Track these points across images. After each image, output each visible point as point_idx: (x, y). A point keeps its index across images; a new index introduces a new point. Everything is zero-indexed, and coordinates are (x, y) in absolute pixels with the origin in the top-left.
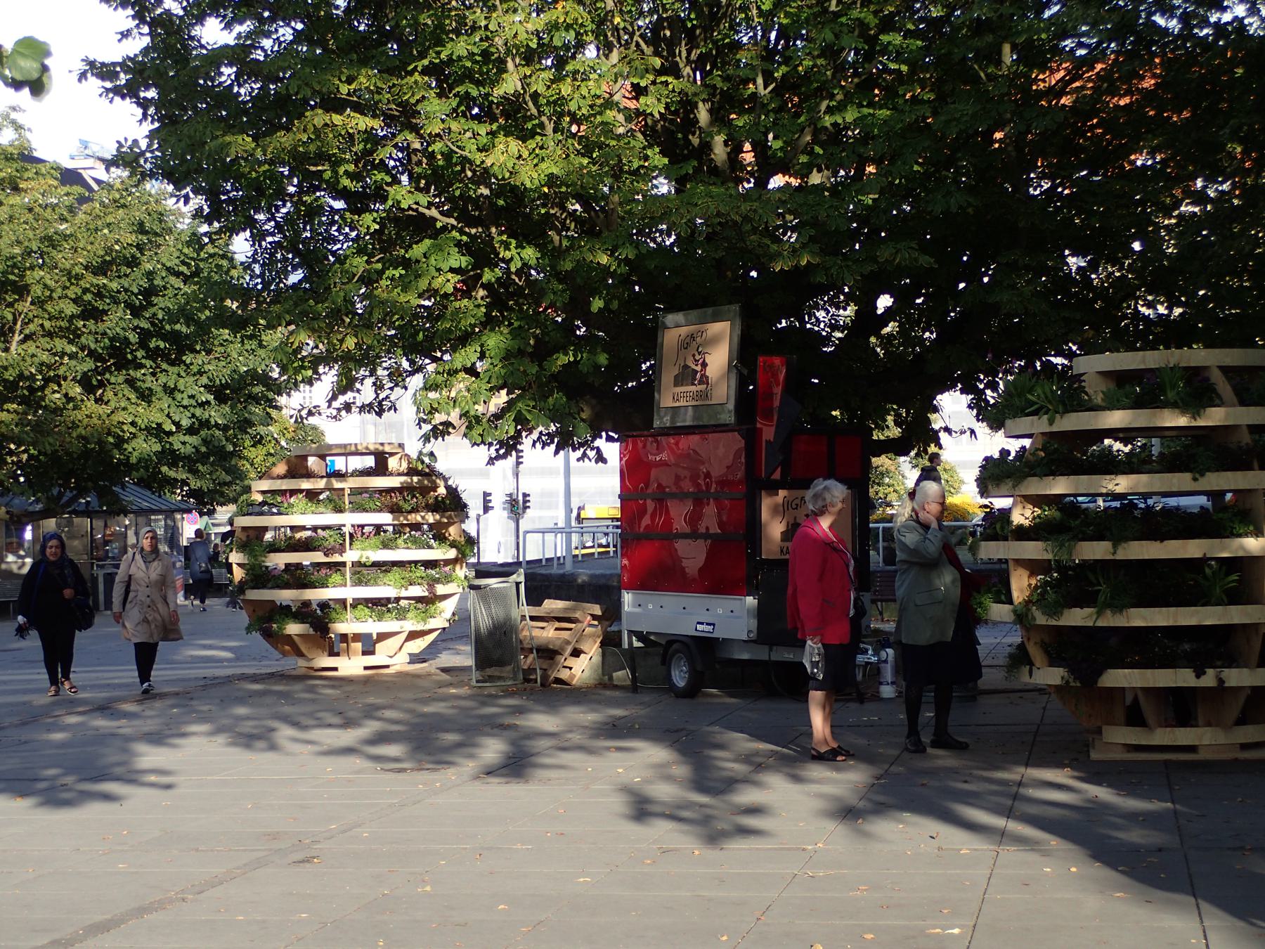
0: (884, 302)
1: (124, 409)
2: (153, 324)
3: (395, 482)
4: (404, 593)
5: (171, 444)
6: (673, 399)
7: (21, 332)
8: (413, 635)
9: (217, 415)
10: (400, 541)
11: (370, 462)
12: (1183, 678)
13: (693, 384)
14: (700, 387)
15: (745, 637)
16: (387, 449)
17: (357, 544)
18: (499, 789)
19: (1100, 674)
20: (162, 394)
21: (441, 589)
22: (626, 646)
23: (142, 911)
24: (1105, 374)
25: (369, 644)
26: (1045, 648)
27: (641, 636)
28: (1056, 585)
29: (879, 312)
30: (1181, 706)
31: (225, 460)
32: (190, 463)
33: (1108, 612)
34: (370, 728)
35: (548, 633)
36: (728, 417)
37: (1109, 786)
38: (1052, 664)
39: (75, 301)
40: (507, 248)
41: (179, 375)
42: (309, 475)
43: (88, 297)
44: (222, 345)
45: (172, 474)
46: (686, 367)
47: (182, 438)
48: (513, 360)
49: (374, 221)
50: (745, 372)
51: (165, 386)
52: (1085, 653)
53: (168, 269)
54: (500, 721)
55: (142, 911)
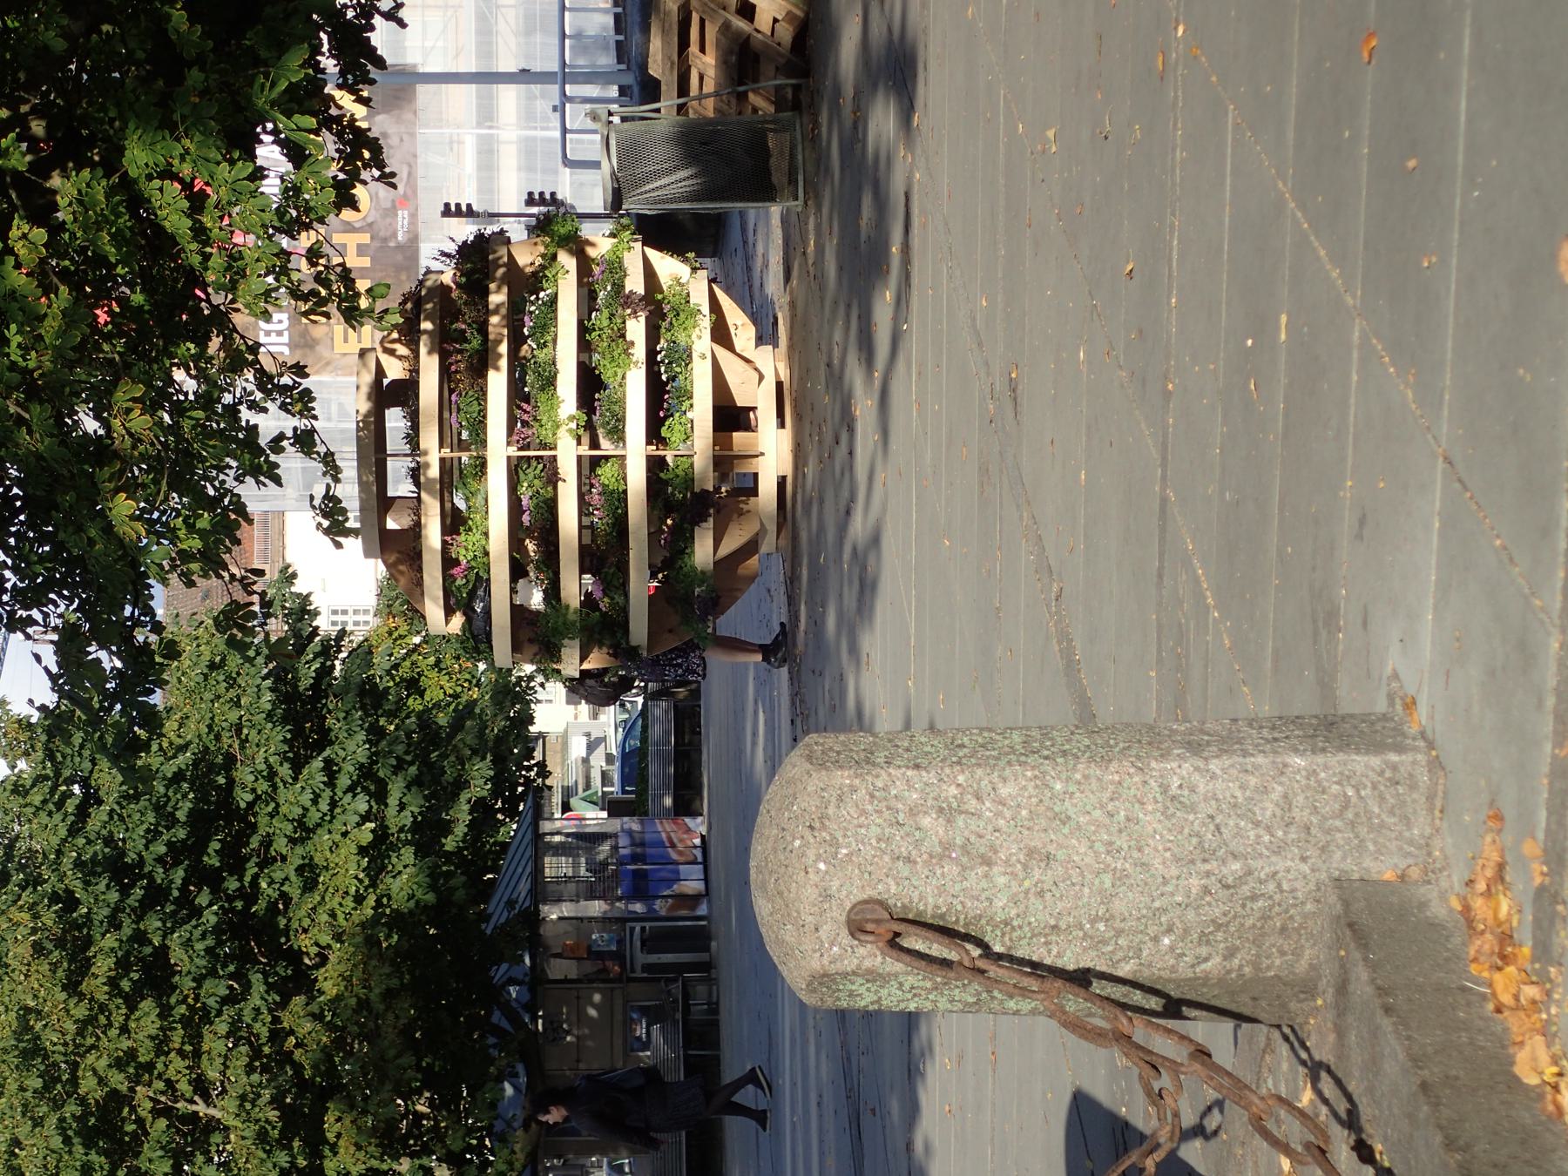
1: (333, 915)
2: (176, 863)
3: (430, 369)
4: (639, 352)
5: (401, 830)
7: (192, 1102)
8: (721, 334)
9: (353, 749)
10: (542, 355)
16: (368, 378)
18: (936, 84)
20: (309, 846)
21: (635, 283)
23: (1071, 667)
25: (731, 418)
31: (437, 734)
32: (439, 790)
34: (855, 375)
35: (706, 64)
39: (132, 1008)
41: (271, 816)
43: (126, 985)
44: (218, 737)
45: (460, 830)
47: (392, 811)
48: (177, 117)
53: (73, 831)
54: (848, 123)
55: (1071, 667)
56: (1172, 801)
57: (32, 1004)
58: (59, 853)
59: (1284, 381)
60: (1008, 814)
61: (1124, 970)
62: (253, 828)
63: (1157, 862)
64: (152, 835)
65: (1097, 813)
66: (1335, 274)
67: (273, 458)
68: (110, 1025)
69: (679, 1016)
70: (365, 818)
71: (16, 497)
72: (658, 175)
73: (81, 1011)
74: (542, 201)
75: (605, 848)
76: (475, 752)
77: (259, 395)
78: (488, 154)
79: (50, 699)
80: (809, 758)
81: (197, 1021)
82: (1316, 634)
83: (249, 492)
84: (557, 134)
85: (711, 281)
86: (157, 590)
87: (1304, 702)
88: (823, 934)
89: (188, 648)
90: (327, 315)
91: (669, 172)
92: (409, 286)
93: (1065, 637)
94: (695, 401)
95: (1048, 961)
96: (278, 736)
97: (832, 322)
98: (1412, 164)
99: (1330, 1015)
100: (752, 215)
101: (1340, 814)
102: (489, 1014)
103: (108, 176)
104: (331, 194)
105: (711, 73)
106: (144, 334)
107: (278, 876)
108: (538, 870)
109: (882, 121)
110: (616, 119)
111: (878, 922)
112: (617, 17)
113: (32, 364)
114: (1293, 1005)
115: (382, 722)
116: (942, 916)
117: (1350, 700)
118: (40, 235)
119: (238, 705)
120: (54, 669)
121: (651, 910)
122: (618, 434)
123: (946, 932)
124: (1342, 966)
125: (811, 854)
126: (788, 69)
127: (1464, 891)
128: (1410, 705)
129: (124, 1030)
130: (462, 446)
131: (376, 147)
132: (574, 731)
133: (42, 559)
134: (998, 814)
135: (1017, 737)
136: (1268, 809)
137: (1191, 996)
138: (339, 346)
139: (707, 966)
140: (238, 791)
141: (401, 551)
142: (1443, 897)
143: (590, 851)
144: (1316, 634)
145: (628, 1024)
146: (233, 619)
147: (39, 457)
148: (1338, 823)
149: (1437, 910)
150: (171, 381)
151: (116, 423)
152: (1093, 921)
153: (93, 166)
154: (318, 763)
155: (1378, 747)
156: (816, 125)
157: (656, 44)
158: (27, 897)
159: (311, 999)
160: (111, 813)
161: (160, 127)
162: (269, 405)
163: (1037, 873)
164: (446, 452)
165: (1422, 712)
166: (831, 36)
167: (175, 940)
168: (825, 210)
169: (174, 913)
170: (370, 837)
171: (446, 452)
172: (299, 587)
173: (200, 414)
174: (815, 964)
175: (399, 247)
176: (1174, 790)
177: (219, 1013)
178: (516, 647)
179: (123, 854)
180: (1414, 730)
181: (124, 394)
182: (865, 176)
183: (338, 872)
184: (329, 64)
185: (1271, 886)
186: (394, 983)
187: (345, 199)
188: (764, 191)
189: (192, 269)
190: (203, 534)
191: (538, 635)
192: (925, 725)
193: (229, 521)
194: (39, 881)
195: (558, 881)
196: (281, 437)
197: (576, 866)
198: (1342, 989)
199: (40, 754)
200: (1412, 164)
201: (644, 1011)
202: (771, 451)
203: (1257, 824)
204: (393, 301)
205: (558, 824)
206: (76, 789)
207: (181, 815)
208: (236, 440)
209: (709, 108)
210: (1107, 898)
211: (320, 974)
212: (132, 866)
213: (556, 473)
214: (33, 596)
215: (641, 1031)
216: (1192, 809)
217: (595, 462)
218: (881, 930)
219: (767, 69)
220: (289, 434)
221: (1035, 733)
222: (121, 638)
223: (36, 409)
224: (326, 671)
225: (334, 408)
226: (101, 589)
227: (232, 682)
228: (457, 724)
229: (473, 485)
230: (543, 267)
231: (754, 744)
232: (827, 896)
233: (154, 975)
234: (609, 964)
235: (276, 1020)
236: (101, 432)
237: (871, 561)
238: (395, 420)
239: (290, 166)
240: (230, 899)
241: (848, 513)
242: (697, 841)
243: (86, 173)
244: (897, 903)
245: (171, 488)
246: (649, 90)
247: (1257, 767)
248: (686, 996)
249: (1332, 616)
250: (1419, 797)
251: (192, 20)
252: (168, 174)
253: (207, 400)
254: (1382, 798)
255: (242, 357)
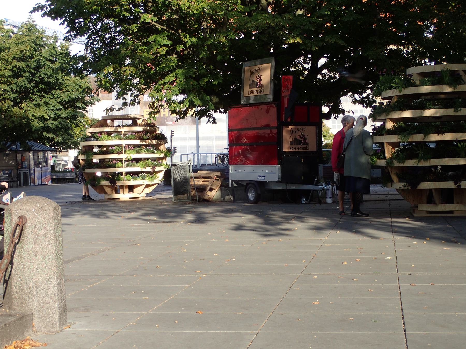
0: (322, 61)
1: (30, 110)
2: (40, 79)
4: (144, 170)
5: (47, 124)
6: (249, 93)
8: (148, 186)
9: (64, 114)
10: (143, 151)
11: (130, 122)
12: (450, 185)
13: (256, 87)
14: (259, 89)
15: (277, 180)
16: (138, 117)
17: (127, 152)
18: (197, 227)
19: (419, 184)
20: (44, 105)
21: (157, 169)
22: (230, 186)
23: (79, 258)
24: (420, 74)
25: (131, 188)
26: (398, 175)
27: (236, 182)
28: (402, 151)
29: (319, 66)
30: (447, 196)
32: (56, 131)
33: (422, 160)
35: (200, 182)
36: (270, 98)
37: (425, 222)
38: (400, 181)
39: (10, 70)
40: (186, 37)
42: (107, 126)
43: (15, 69)
44: (66, 87)
45: (48, 135)
46: (253, 81)
49: (136, 27)
50: (276, 82)
51: (45, 102)
52: (412, 177)
53: (46, 59)
54: (189, 210)
55: (79, 258)
56: (48, 280)
57: (11, 50)
58: (41, 56)
59: (135, 298)
60: (45, 247)
61: (13, 272)
62: (47, 94)
63: (35, 277)
64: (45, 74)
65: (45, 265)
66: (156, 308)
67: (121, 98)
68: (6, 66)
69: (10, 180)
70: (50, 116)
71: (112, 48)
72: (179, 173)
73: (10, 60)
74: (175, 150)
75: (45, 165)
76: (64, 138)
77: (134, 95)
78: (184, 139)
79: (72, 54)
80: (56, 207)
81: (9, 84)
82: (84, 307)
83: (114, 94)
84: (188, 153)
85: (158, 184)
86: (94, 75)
87: (69, 305)
88: (20, 211)
89: (83, 81)
90: (150, 108)
91: (179, 175)
92: (156, 125)
93: (85, 256)
94: (135, 181)
95: (15, 256)
96: (66, 99)
97: (150, 208)
98: (177, 322)
99: (5, 313)
100: (171, 191)
101: (46, 314)
102: (10, 142)
103: (176, 66)
104: (173, 109)
105: (199, 183)
106: (145, 72)
107: (37, 99)
108: (40, 151)
109: (190, 217)
110: (189, 164)
111: (22, 222)
112: (210, 164)
113: (138, 51)
114: (7, 306)
115: (70, 120)
116: (24, 235)
117: (70, 315)
118: (164, 53)
119: (72, 91)
120: (78, 55)
121: (32, 174)
122: (127, 166)
123: (20, 235)
124: (15, 315)
125: (36, 208)
126: (200, 198)
127: (31, 339)
128: (69, 327)
129: (6, 69)
130: (125, 135)
131: (182, 118)
132: (68, 158)
133: (100, 53)
134: (45, 245)
135: (61, 248)
136: (47, 299)
137: (8, 285)
138: (145, 111)
139: (20, 185)
140: (55, 91)
141: (103, 123)
142: (29, 335)
143: (44, 161)
144: (84, 307)
145: (7, 170)
146: (89, 90)
147: (120, 52)
148: (44, 313)
149: (27, 334)
150: (136, 78)
151: (127, 68)
152: (23, 265)
153: (178, 63)
154: (61, 107)
155: (60, 321)
156: (189, 204)
157: (204, 172)
158: (32, 49)
159: (12, 106)
160: (50, 66)
161: (186, 76)
162: (132, 97)
163: (33, 253)
164: (123, 132)
165: (67, 329)
166: (206, 206)
167: (24, 78)
168: (172, 206)
169: (29, 79)
170: (46, 118)
171: (123, 132)
172: (96, 103)
173: (129, 84)
174: (13, 209)
175: (165, 122)
176: (50, 280)
177: (9, 88)
178: (84, 146)
179: (41, 68)
180: (64, 328)
181: (133, 69)
182: (179, 214)
183: (38, 111)
184: (199, 108)
185: (31, 300)
186: (16, 123)
187: (173, 112)
188: (176, 194)
189: (158, 82)
190: (105, 85)
191: (88, 151)
192: (64, 229)
193: (109, 90)
194: (35, 51)
195: (37, 156)
196: (126, 100)
197: (41, 159)
198: (10, 315)
199: (62, 52)
200: (177, 322)
201: (11, 173)
202: (125, 196)
203: (44, 297)
204: (153, 121)
205: (49, 155)
206: (55, 59)
207: (50, 80)
208: (125, 91)
209: (192, 183)
210: (28, 267)
211: (17, 108)
212: (39, 70)
213: (119, 154)
214: (92, 51)
215: (7, 172)
216: (47, 284)
217: (121, 161)
218: (21, 222)
219: (200, 194)
220: (126, 101)
221: (62, 252)
222: (85, 67)
223: (130, 52)
224: (79, 108)
225: (133, 109)
226: (94, 64)
227: (77, 90)
228: (69, 135)
229: (117, 137)
230: (160, 151)
231: (66, 194)
232: (27, 211)
233: (17, 75)
234: (20, 166)
235: (8, 99)
236: (126, 64)
237: (103, 217)
238: (130, 122)
239: (179, 101)
240: (32, 90)
241: (113, 212)
242: (46, 183)
243: (176, 62)
244: (26, 225)
245: (115, 78)
246: (195, 171)
247: (55, 297)
248: (14, 181)
249: (87, 310)
250: (50, 329)
251: (206, 82)
252: (176, 78)
253: (132, 85)
254: (50, 322)
255: (141, 91)
